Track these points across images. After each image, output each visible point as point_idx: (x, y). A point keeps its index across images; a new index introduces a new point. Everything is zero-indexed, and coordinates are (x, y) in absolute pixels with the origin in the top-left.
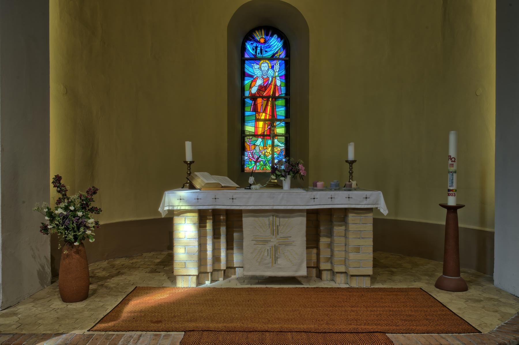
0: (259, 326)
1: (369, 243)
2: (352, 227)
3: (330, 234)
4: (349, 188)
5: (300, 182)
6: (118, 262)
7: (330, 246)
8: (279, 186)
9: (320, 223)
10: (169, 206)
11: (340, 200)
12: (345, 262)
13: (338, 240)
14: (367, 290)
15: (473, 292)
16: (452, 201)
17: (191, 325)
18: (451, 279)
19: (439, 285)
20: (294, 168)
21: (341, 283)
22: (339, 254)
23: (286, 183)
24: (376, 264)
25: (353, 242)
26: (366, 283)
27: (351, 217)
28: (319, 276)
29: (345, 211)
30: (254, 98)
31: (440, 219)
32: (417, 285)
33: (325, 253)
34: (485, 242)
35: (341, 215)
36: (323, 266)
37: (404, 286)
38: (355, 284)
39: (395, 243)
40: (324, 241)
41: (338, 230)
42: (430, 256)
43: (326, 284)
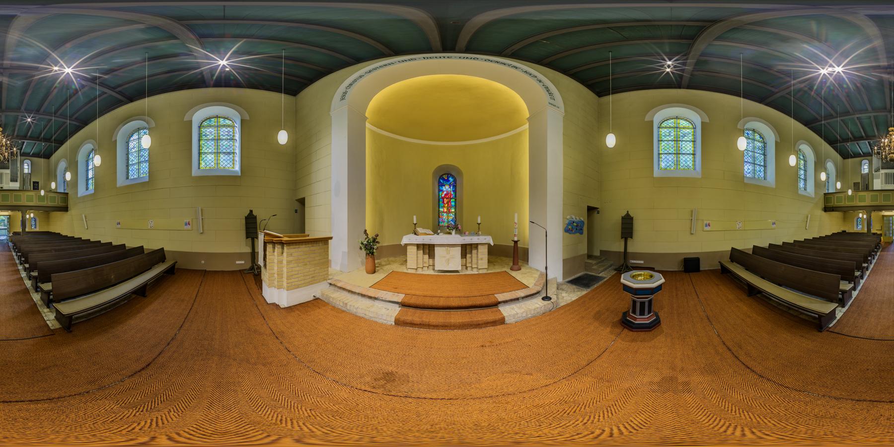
0: (438, 294)
1: (486, 256)
2: (479, 250)
3: (471, 253)
4: (479, 235)
5: (460, 232)
6: (391, 259)
7: (471, 257)
8: (450, 233)
9: (466, 250)
10: (34, 310)
11: (475, 240)
12: (477, 263)
13: (474, 255)
14: (486, 274)
15: (523, 270)
16: (516, 239)
17: (409, 292)
18: (516, 267)
19: (512, 269)
20: (456, 227)
21: (475, 272)
22: (474, 260)
23: (453, 232)
24: (489, 262)
25: (480, 256)
26: (485, 271)
27: (479, 247)
28: (467, 268)
29: (477, 245)
30: (443, 198)
31: (512, 244)
32: (504, 270)
33: (469, 260)
34: (526, 252)
35: (476, 246)
36: (468, 265)
37: (499, 271)
38: (481, 272)
39: (495, 253)
40: (468, 256)
41: (474, 252)
42: (507, 256)
43: (469, 272)
